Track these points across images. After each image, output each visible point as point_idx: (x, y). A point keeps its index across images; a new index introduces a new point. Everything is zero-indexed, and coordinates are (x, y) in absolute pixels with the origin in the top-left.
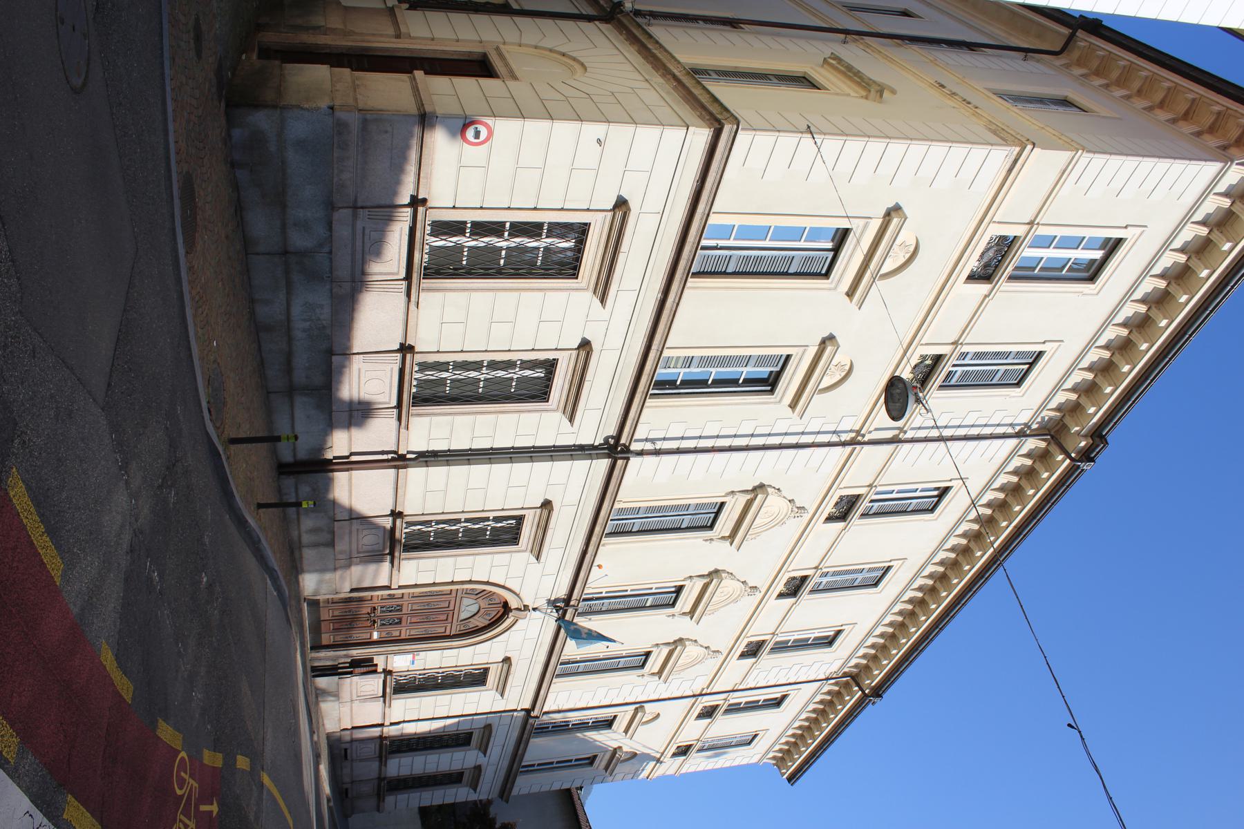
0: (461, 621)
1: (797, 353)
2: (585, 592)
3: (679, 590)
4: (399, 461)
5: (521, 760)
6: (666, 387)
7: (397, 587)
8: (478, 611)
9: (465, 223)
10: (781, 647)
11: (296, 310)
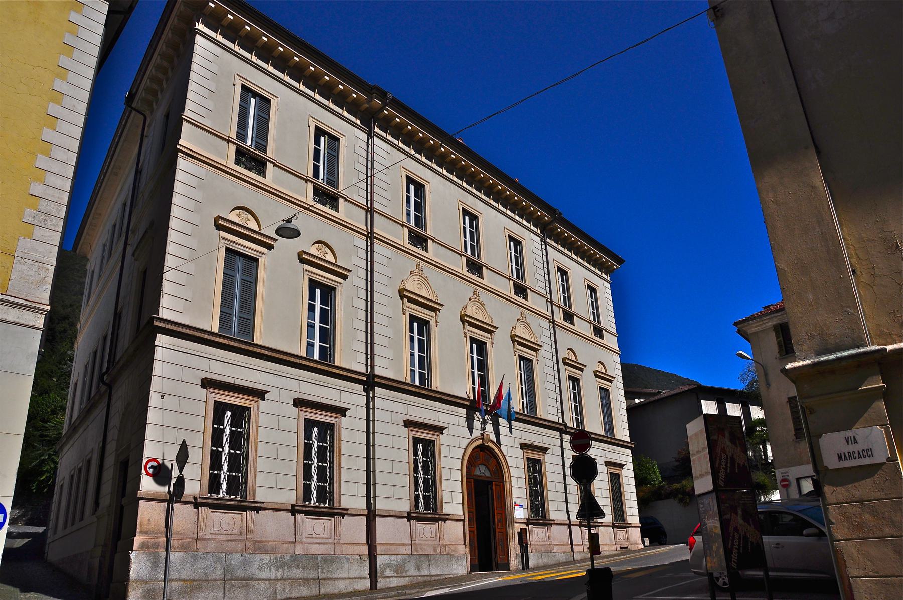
1: (308, 275)
2: (522, 412)
3: (521, 358)
4: (371, 515)
6: (327, 353)
8: (484, 465)
9: (210, 474)
10: (520, 273)
11: (264, 575)
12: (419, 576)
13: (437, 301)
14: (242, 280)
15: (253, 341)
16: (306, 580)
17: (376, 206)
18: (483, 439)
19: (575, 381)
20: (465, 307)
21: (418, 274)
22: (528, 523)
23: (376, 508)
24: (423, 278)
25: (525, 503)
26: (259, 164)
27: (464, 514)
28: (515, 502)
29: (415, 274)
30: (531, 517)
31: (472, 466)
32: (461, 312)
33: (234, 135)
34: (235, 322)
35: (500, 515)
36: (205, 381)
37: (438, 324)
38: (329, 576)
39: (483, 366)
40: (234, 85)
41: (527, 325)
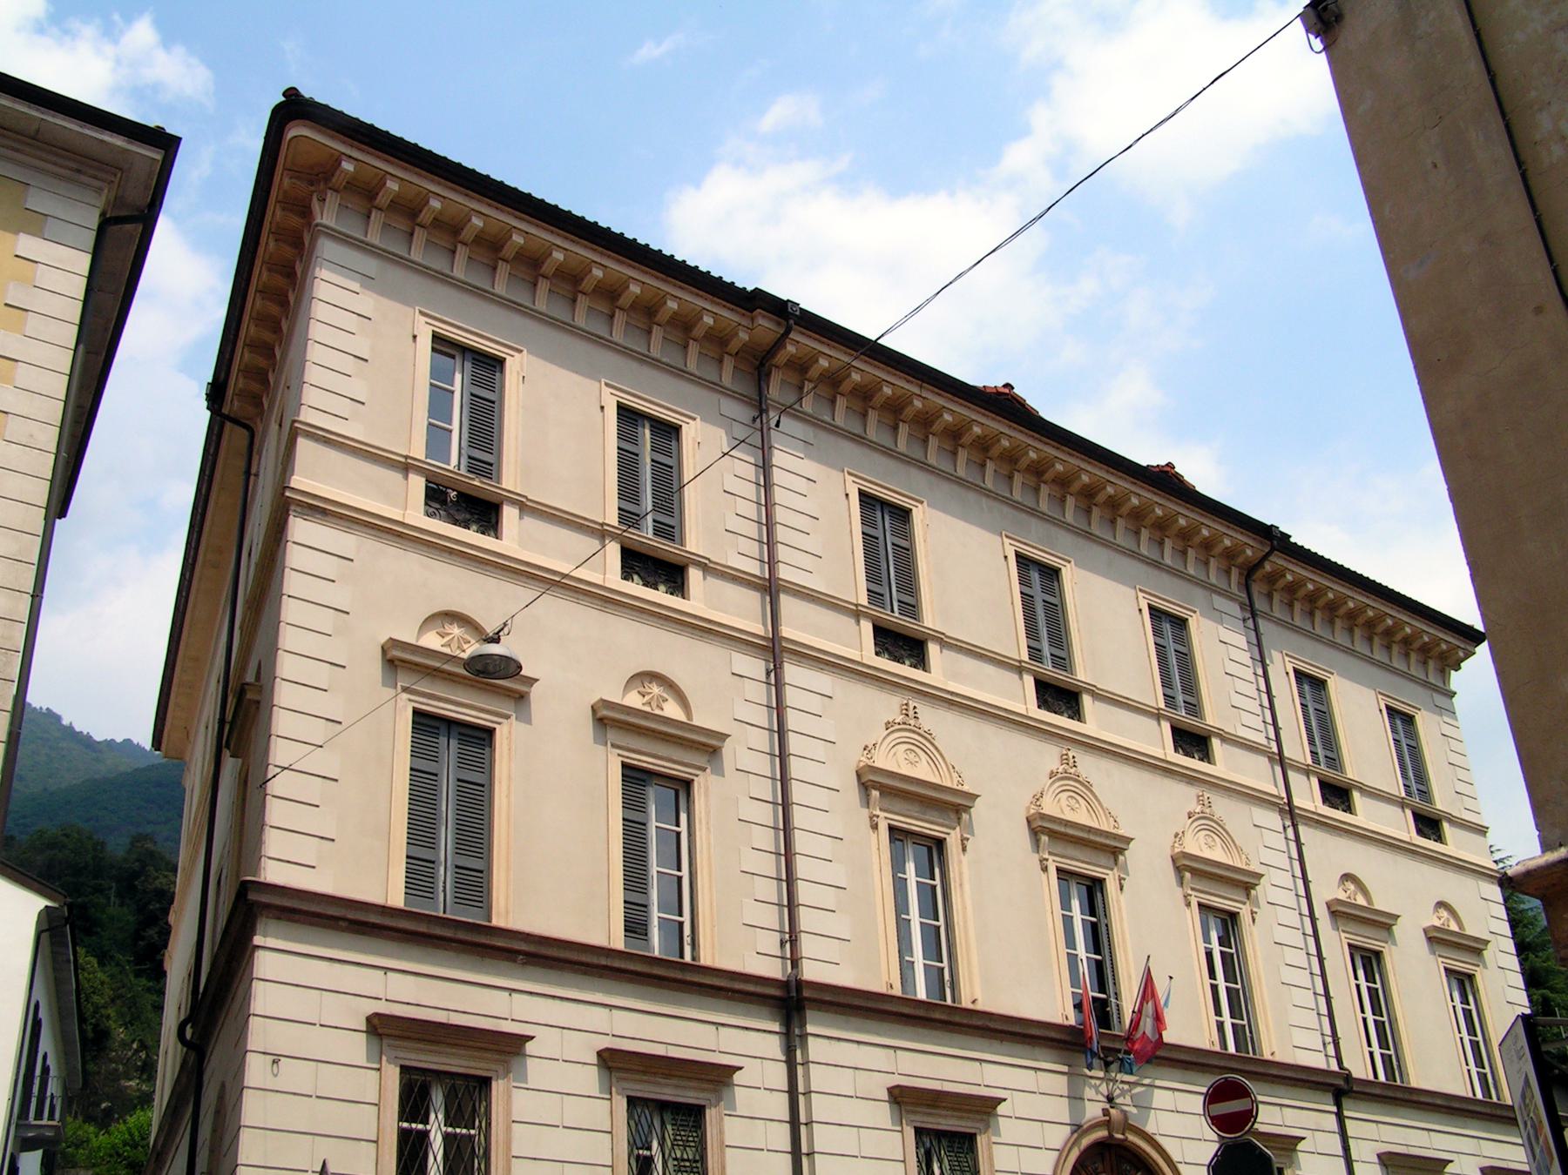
13: (960, 788)
14: (459, 780)
15: (490, 921)
17: (784, 573)
19: (1369, 961)
20: (1038, 798)
26: (671, 574)
29: (897, 727)
33: (612, 518)
34: (444, 876)
36: (376, 1021)
37: (969, 845)
39: (1098, 937)
41: (924, 742)
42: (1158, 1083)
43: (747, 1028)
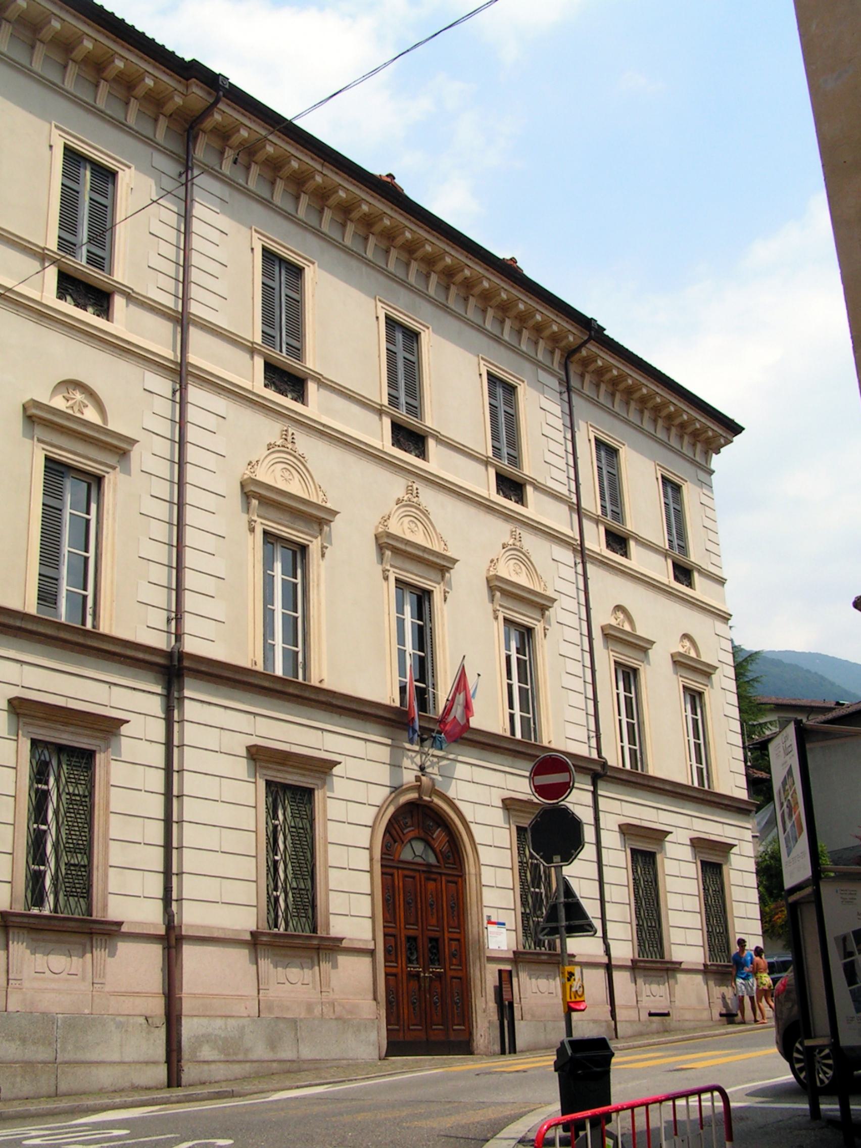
0: (438, 862)
1: (43, 449)
5: (691, 788)
7: (373, 942)
12: (274, 1061)
13: (324, 504)
16: (28, 1065)
17: (195, 309)
18: (420, 786)
20: (386, 519)
21: (283, 449)
22: (518, 958)
23: (184, 922)
24: (295, 457)
25: (512, 919)
27: (374, 939)
28: (489, 917)
30: (524, 947)
31: (395, 842)
32: (377, 527)
33: (53, 244)
35: (456, 943)
38: (80, 1056)
39: (423, 638)
40: (51, 147)
42: (460, 758)
43: (134, 689)
